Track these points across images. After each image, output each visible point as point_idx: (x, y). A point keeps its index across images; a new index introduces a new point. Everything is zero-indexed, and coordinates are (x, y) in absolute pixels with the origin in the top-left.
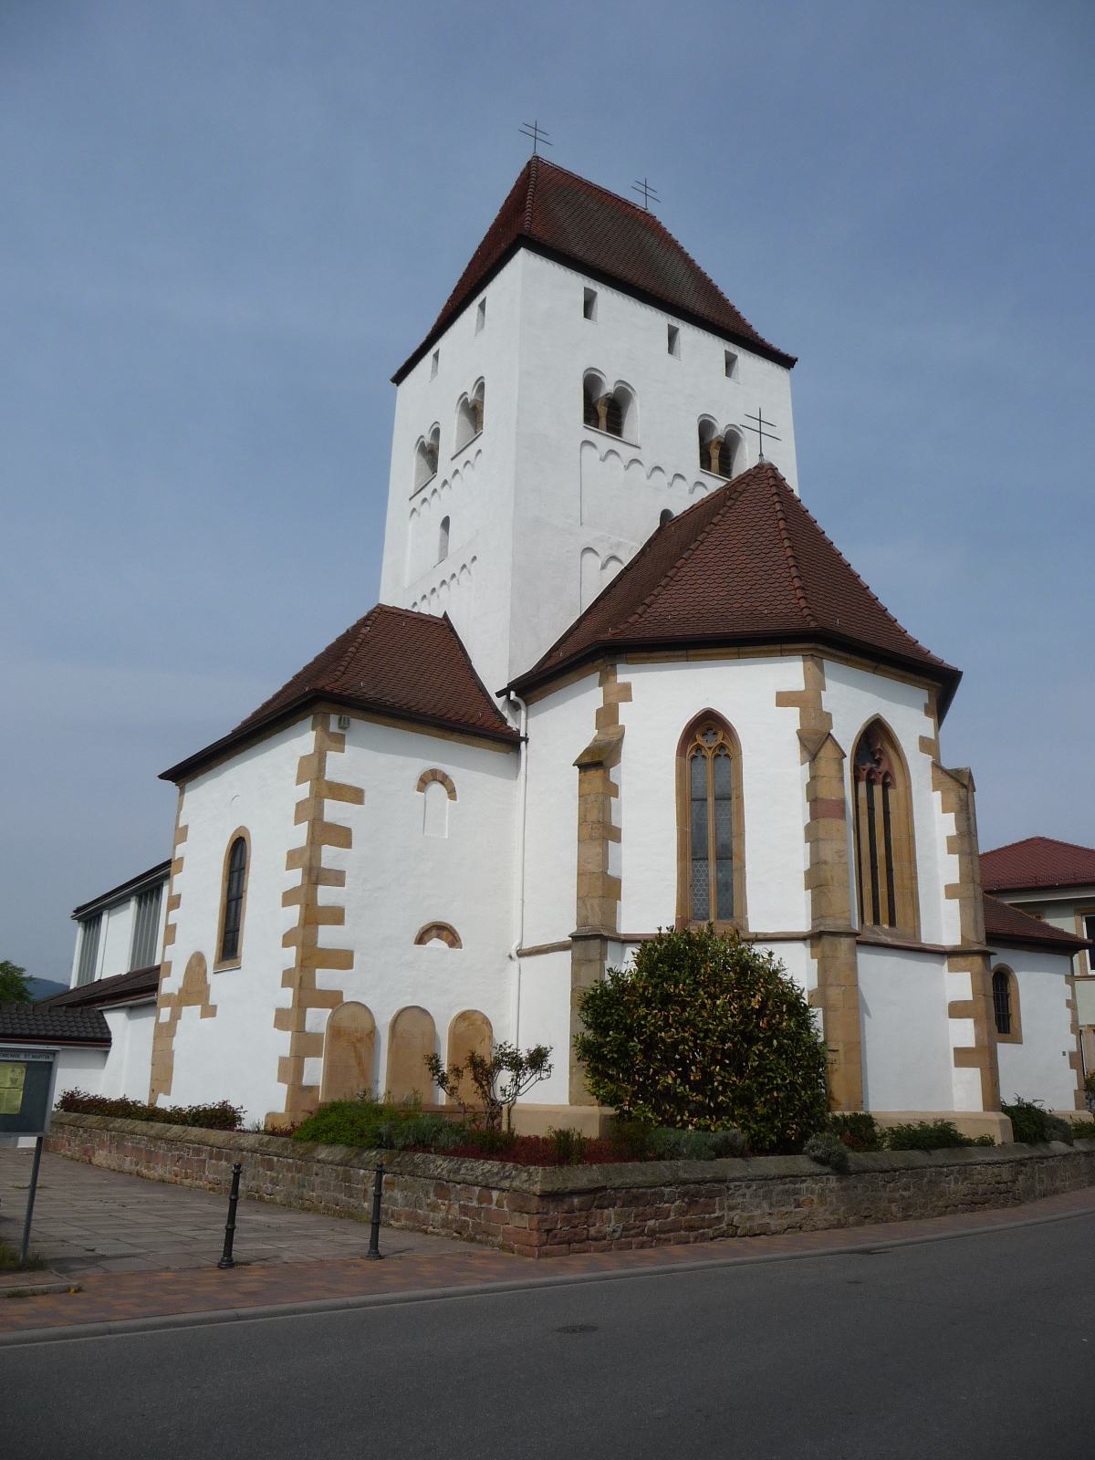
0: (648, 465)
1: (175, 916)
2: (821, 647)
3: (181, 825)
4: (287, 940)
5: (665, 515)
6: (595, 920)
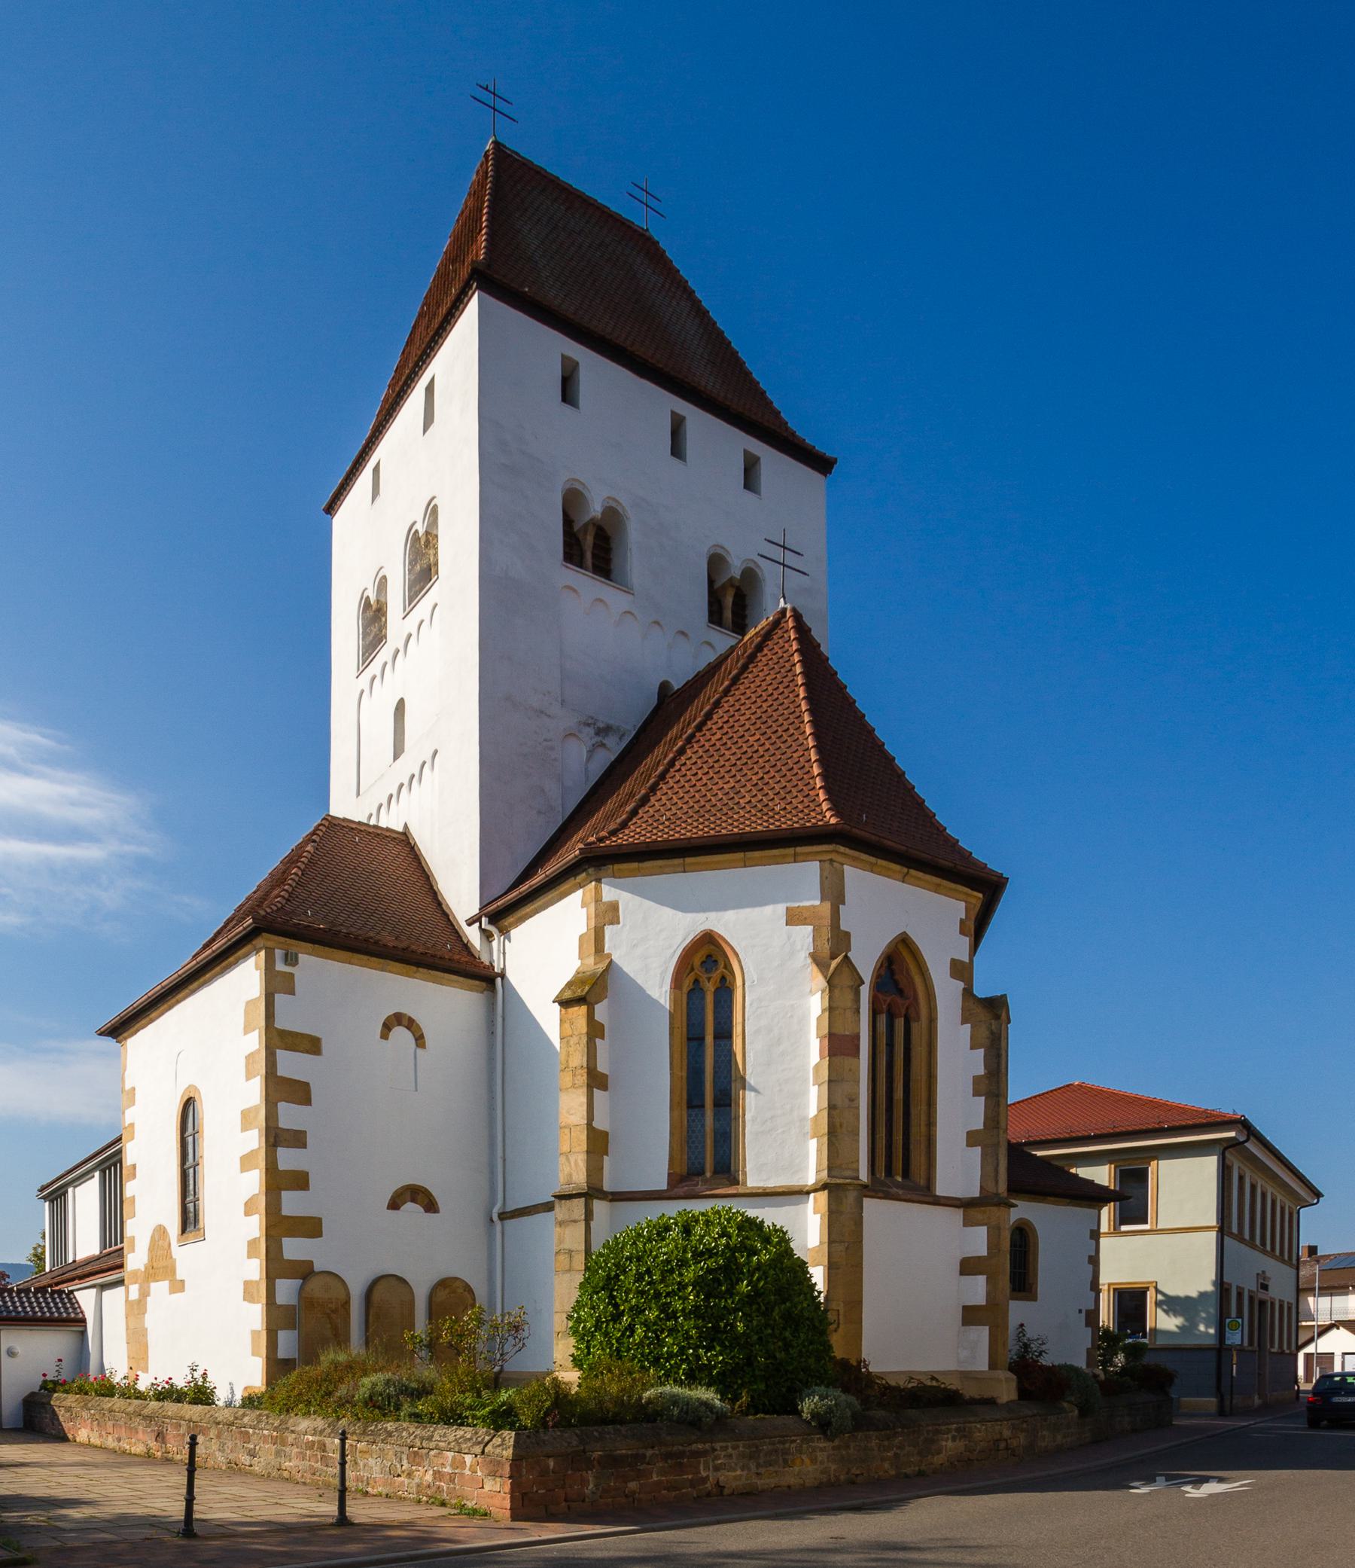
2: (842, 849)
5: (664, 686)
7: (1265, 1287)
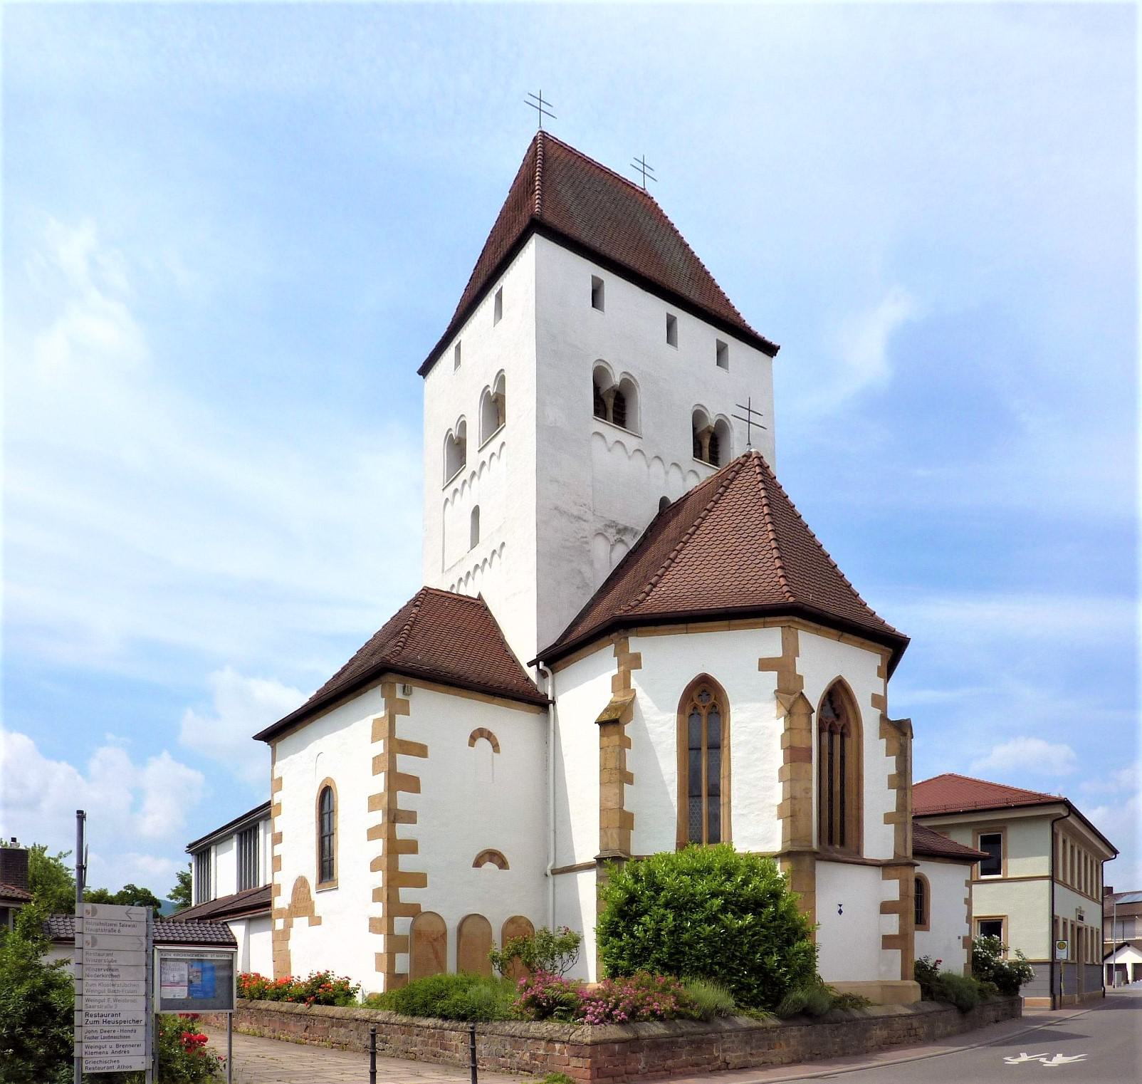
0: (650, 455)
1: (279, 849)
3: (276, 777)
4: (374, 867)
5: (664, 501)
6: (614, 845)
7: (1081, 918)
